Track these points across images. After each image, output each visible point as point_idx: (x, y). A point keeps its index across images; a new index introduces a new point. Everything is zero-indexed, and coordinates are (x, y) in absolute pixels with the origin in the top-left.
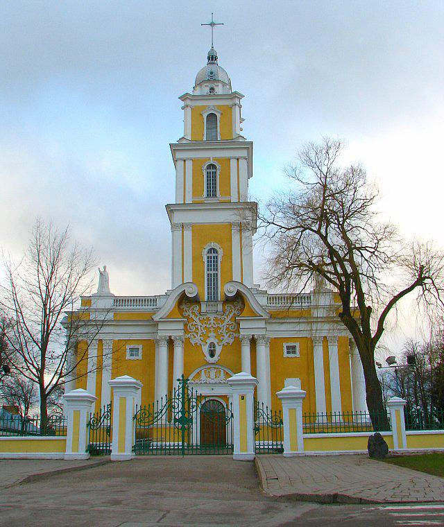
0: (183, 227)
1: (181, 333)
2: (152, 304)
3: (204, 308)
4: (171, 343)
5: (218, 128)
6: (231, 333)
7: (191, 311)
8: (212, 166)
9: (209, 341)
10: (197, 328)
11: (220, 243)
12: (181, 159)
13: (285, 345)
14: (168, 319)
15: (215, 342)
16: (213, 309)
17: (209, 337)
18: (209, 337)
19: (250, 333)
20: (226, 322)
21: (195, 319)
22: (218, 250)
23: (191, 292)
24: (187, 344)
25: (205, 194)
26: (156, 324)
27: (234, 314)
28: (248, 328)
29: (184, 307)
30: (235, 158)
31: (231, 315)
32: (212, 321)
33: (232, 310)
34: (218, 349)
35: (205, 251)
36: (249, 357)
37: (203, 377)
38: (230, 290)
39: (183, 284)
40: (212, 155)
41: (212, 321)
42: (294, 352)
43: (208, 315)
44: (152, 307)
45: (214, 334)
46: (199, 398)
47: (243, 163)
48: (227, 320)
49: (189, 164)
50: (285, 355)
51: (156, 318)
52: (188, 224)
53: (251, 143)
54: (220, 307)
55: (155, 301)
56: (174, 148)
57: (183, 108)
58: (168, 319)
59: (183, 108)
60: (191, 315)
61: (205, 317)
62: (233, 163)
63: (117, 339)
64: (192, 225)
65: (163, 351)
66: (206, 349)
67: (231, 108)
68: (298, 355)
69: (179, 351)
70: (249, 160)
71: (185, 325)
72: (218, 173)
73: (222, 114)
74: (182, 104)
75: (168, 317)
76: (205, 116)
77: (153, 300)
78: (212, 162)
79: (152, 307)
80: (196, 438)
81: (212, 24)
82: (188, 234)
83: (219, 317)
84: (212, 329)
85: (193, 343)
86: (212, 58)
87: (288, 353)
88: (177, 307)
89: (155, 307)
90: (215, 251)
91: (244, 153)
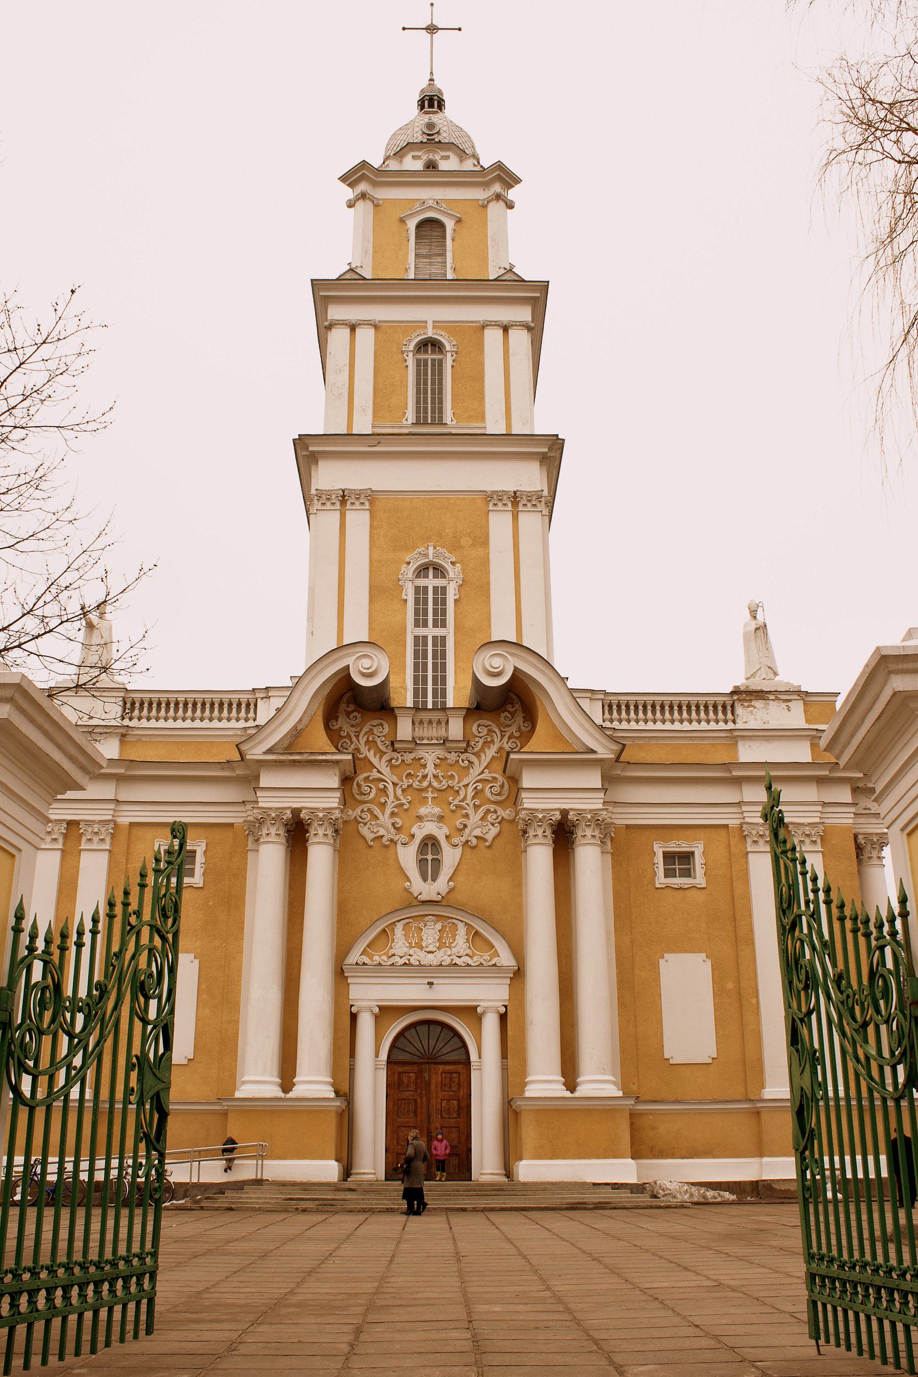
0: (343, 502)
1: (332, 801)
2: (243, 714)
3: (405, 729)
4: (297, 833)
5: (449, 255)
6: (492, 807)
7: (367, 741)
8: (430, 345)
9: (420, 831)
10: (384, 791)
11: (455, 547)
12: (343, 323)
13: (659, 850)
14: (292, 754)
15: (440, 832)
16: (434, 732)
17: (420, 818)
18: (420, 818)
19: (554, 804)
20: (474, 773)
21: (375, 761)
22: (448, 567)
23: (369, 670)
24: (344, 834)
25: (411, 416)
26: (250, 780)
27: (500, 749)
28: (549, 791)
29: (342, 724)
30: (497, 324)
31: (491, 752)
32: (430, 770)
33: (493, 742)
34: (450, 857)
35: (410, 571)
36: (33, 695)
37: (400, 945)
38: (495, 670)
39: (199, 1161)
40: (430, 317)
41: (430, 770)
42: (687, 873)
43: (421, 753)
44: (242, 724)
45: (437, 810)
46: (385, 1013)
47: (520, 339)
48: (477, 769)
49: (366, 336)
50: (661, 880)
51: (256, 752)
52: (358, 494)
53: (544, 287)
54: (456, 729)
55: (251, 706)
56: (324, 293)
57: (351, 205)
58: (292, 754)
59: (351, 205)
60: (364, 750)
61: (408, 757)
62: (493, 337)
63: (124, 820)
64: (371, 498)
65: (269, 859)
66: (408, 856)
67: (485, 207)
68: (700, 879)
69: (320, 857)
70: (536, 330)
71: (346, 780)
72: (449, 361)
73: (459, 221)
74: (349, 194)
75: (288, 750)
76: (412, 224)
77: (244, 704)
78: (430, 333)
79: (242, 724)
80: (372, 1160)
81: (432, 29)
82: (359, 521)
83: (453, 757)
84: (430, 795)
85: (369, 836)
86: (431, 102)
87: (669, 873)
88: (320, 719)
89: (251, 723)
90: (439, 571)
91: (524, 314)
